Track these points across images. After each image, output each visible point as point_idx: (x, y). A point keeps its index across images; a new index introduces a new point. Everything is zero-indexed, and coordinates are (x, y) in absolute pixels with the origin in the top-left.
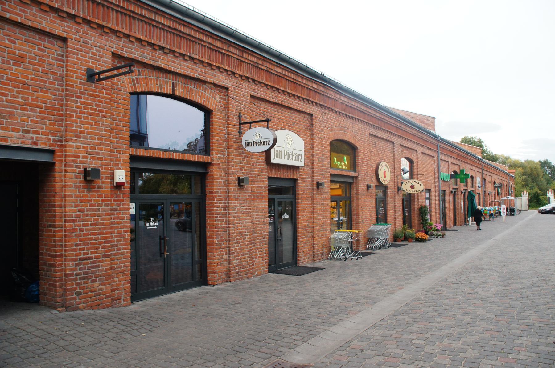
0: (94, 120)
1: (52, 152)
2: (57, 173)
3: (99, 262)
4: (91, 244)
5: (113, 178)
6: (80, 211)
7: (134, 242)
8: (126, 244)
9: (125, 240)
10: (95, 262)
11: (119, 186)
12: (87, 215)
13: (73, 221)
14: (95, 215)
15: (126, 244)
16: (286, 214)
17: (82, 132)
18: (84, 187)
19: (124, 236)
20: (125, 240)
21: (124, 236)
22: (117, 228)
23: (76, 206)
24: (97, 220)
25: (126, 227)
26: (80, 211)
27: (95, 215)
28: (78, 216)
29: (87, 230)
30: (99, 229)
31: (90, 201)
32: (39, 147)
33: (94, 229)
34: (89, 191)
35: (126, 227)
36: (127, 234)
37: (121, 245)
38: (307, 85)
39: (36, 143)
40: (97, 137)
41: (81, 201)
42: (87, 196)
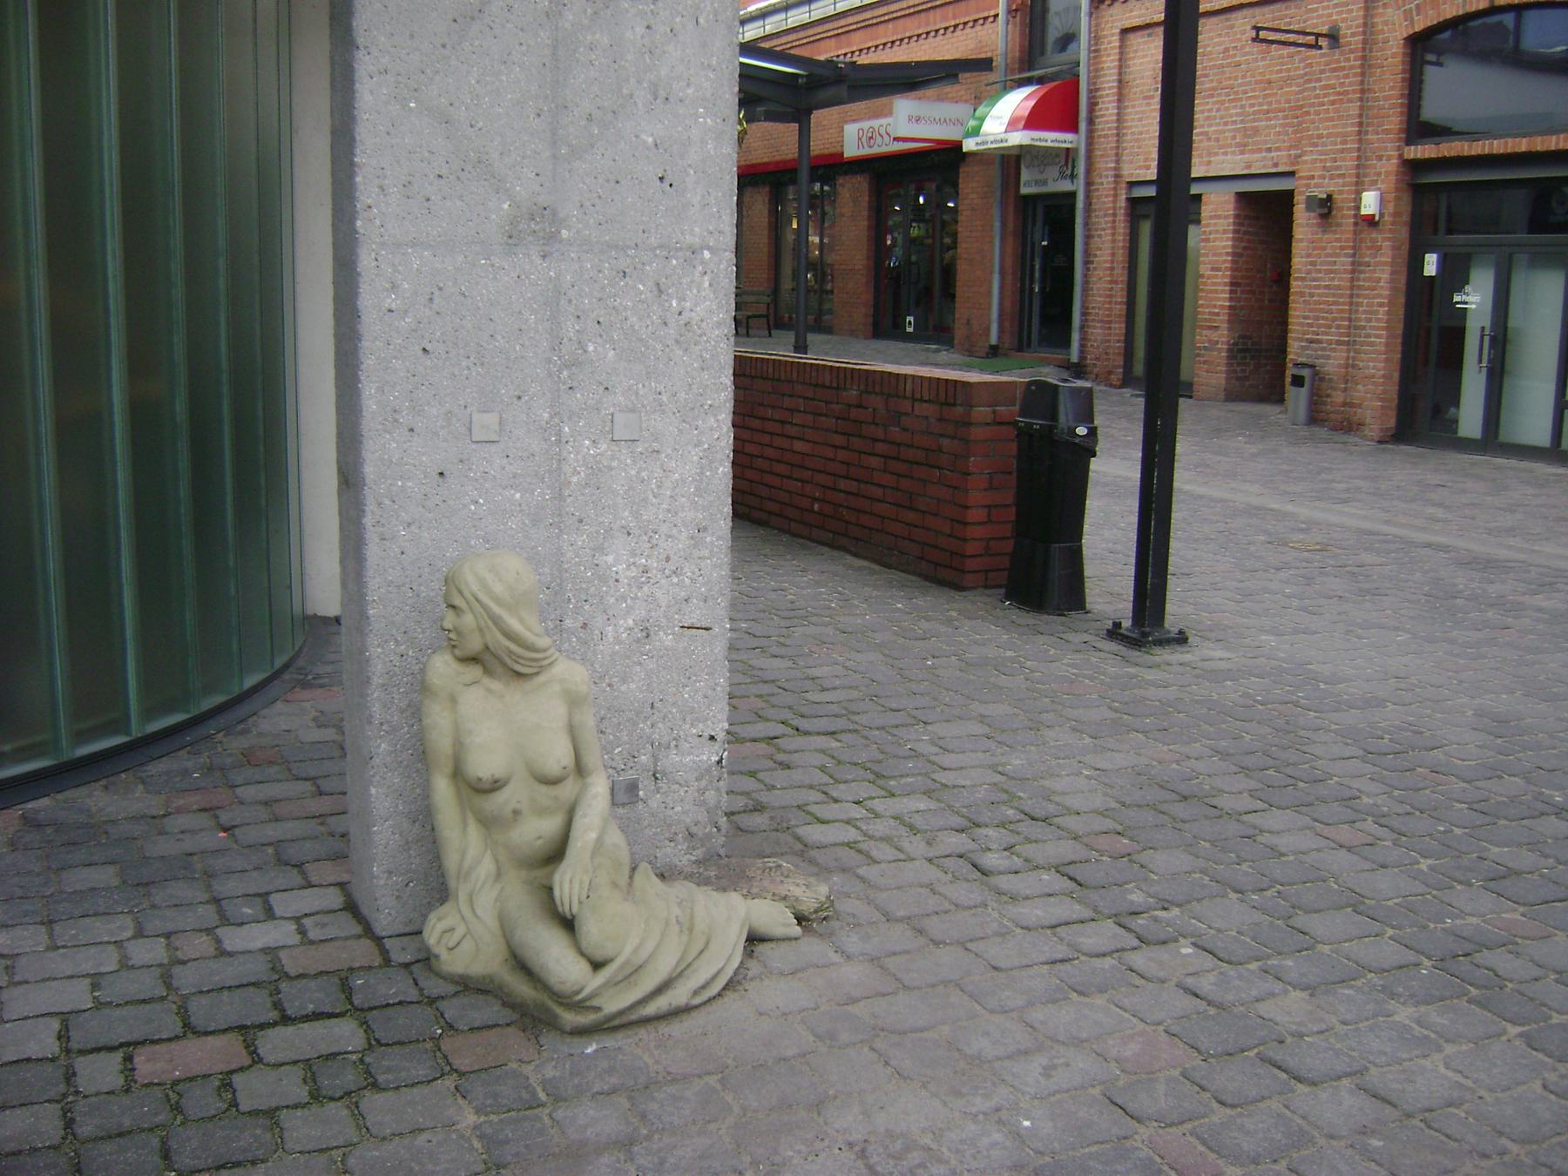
0: (1337, 111)
1: (1291, 174)
2: (1232, 213)
3: (1331, 350)
4: (1323, 318)
5: (1358, 208)
6: (1312, 263)
7: (760, 202)
8: (1378, 328)
9: (1378, 320)
10: (1324, 349)
11: (1370, 221)
12: (1319, 271)
13: (1303, 279)
14: (1331, 272)
15: (1378, 328)
16: (901, 231)
17: (1320, 137)
18: (1318, 225)
19: (1377, 312)
20: (1378, 320)
21: (1377, 312)
22: (1366, 297)
23: (1309, 256)
24: (1333, 279)
25: (1380, 296)
26: (1312, 263)
27: (1331, 272)
28: (1309, 272)
29: (1319, 295)
30: (1334, 295)
31: (1324, 248)
32: (1280, 169)
33: (1327, 296)
34: (1324, 232)
35: (1380, 296)
36: (1381, 309)
37: (1373, 328)
38: (752, 293)
39: (1276, 165)
40: (1339, 140)
41: (1314, 250)
42: (1321, 240)
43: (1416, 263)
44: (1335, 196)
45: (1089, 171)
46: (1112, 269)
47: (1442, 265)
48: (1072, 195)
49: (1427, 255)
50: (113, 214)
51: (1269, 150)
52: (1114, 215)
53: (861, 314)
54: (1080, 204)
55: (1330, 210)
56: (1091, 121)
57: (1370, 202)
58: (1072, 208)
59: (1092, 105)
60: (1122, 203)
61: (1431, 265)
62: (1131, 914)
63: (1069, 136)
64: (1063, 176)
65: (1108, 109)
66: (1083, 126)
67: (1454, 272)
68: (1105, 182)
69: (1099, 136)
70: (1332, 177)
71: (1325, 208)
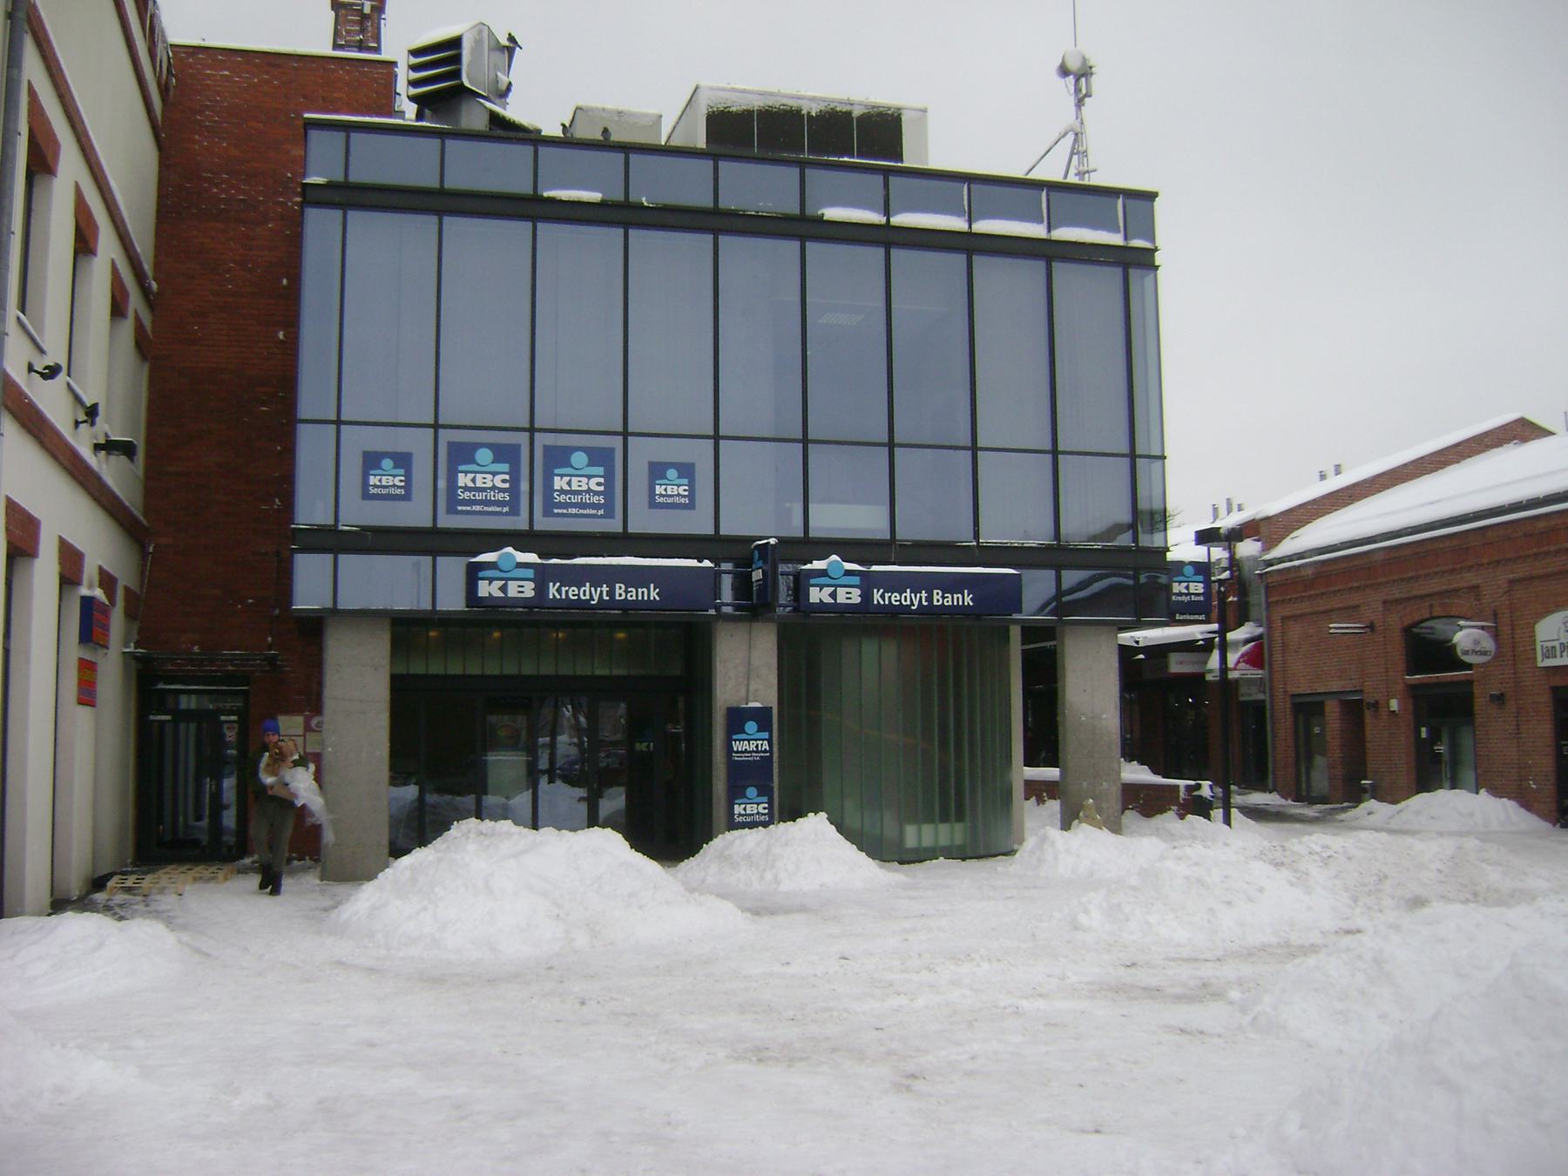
1: (1362, 691)
39: (1355, 687)
43: (1418, 732)
44: (1380, 702)
45: (1271, 689)
46: (1286, 740)
47: (1429, 732)
48: (1264, 701)
49: (629, 531)
50: (186, 785)
51: (1351, 679)
52: (1285, 712)
53: (401, 670)
54: (1268, 707)
55: (1378, 708)
56: (1270, 664)
57: (1394, 705)
58: (1264, 707)
59: (1271, 655)
60: (1288, 705)
61: (1424, 733)
62: (881, 1029)
63: (1260, 672)
64: (1260, 692)
65: (1278, 657)
66: (1266, 666)
67: (1435, 737)
68: (1279, 694)
69: (1550, 746)
70: (1378, 693)
71: (1376, 705)
